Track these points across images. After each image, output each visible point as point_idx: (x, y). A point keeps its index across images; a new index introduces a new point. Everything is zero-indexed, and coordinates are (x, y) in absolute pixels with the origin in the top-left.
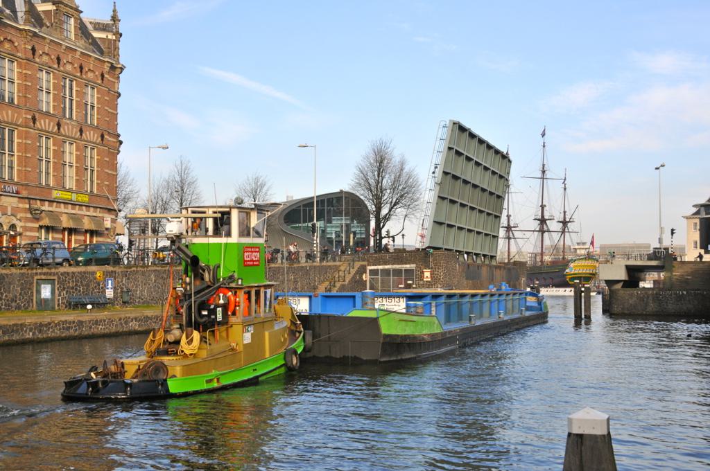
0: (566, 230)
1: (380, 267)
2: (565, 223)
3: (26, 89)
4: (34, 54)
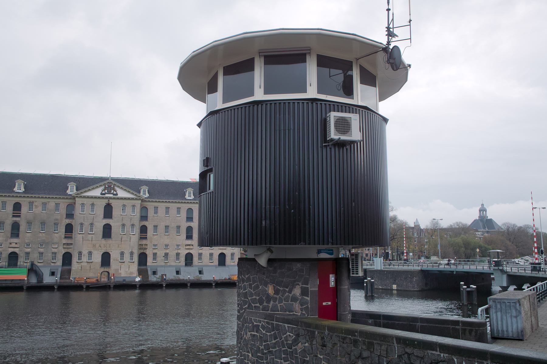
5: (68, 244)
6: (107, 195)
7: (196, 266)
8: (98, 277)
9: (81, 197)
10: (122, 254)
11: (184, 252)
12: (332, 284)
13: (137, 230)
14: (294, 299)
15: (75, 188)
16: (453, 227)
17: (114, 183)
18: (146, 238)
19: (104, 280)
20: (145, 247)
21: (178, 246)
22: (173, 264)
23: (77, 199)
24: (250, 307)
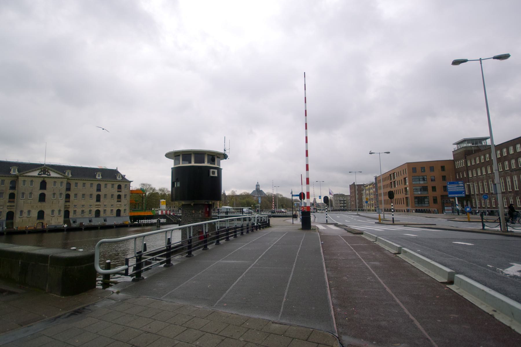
5: (11, 206)
6: (42, 175)
7: (102, 217)
8: (34, 226)
9: (23, 176)
10: (53, 211)
11: (94, 209)
12: (208, 210)
13: (64, 196)
14: (199, 214)
15: (17, 170)
16: (242, 194)
17: (48, 168)
18: (69, 201)
19: (39, 227)
20: (68, 207)
21: (90, 206)
22: (87, 216)
23: (19, 177)
24: (187, 216)
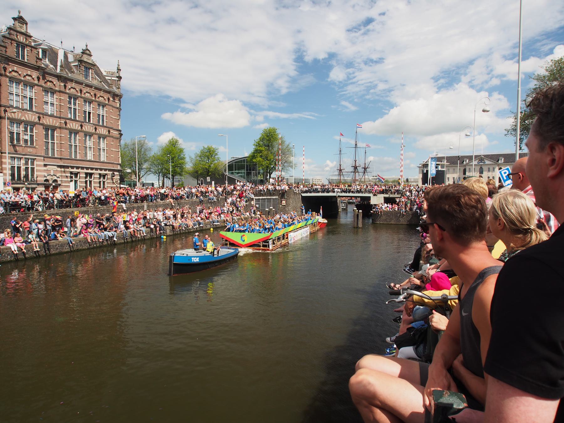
0: (366, 171)
1: (261, 198)
2: (365, 169)
3: (60, 107)
4: (65, 88)
6: (480, 163)
